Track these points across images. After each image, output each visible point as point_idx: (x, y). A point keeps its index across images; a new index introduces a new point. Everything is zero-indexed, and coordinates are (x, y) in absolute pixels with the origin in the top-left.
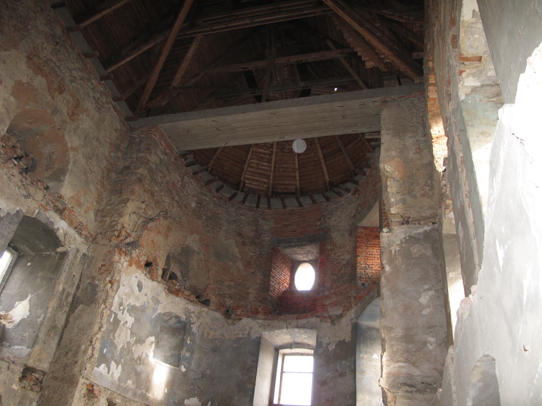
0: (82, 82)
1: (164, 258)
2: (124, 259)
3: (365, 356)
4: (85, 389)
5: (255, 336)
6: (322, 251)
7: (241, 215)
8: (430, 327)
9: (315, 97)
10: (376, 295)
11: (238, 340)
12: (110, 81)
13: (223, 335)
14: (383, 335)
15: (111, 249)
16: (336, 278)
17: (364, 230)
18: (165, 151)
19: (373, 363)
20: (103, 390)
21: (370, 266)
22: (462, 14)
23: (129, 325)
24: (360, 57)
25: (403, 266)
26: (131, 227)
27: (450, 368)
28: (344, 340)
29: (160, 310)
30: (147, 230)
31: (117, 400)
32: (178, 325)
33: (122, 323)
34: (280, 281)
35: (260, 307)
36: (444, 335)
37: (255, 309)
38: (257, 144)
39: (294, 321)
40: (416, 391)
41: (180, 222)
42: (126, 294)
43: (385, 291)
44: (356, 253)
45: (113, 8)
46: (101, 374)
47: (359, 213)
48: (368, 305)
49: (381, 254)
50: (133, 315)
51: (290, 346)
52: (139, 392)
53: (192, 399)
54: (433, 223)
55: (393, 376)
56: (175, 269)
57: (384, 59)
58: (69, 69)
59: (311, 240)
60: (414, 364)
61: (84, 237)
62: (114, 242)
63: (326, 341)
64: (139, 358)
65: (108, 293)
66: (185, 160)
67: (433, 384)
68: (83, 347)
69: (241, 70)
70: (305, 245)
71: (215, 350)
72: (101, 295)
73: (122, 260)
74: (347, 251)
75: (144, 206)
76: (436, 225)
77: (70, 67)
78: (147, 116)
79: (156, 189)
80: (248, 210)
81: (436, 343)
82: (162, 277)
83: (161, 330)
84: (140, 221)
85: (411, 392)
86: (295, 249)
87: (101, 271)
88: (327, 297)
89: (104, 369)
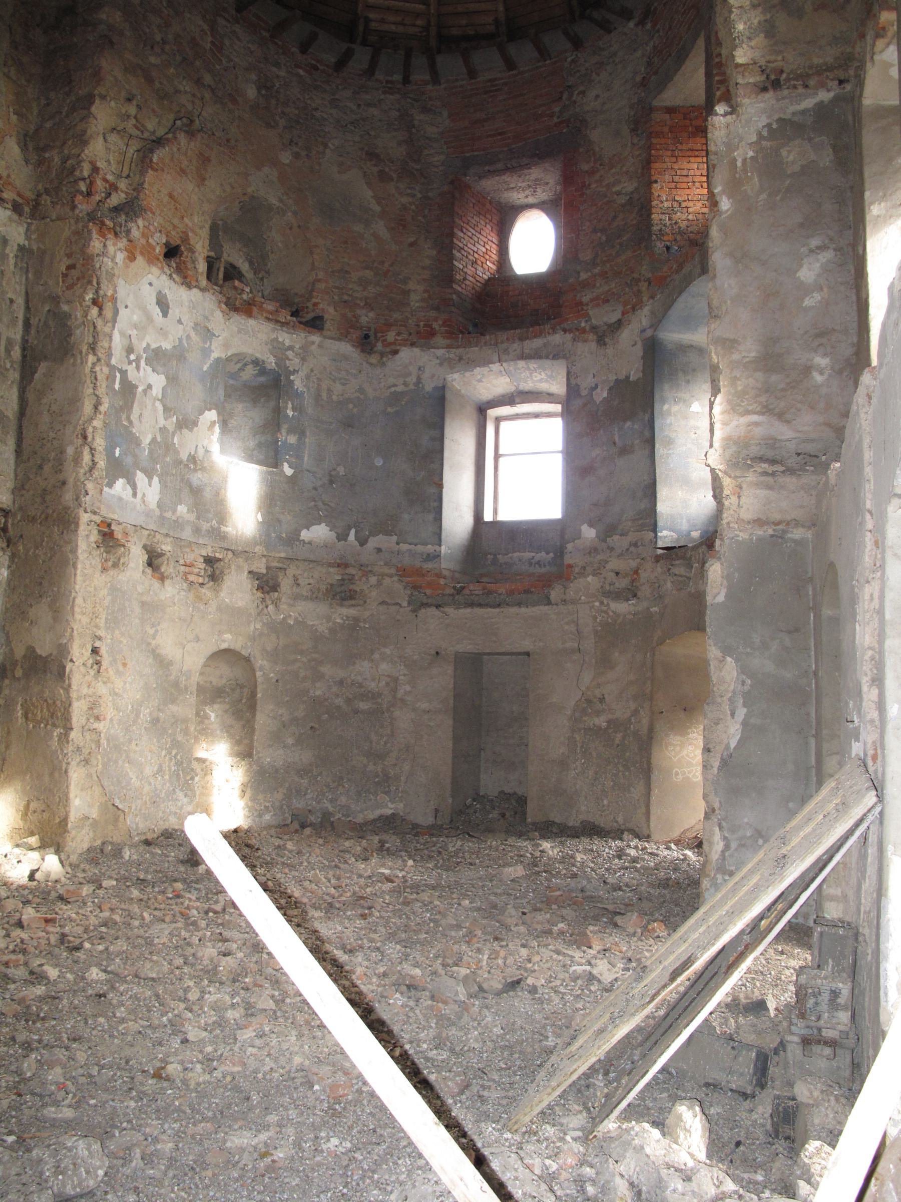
1: (205, 233)
2: (114, 245)
3: (675, 408)
4: (96, 532)
5: (433, 385)
6: (568, 178)
7: (369, 105)
8: (821, 335)
10: (698, 270)
11: (396, 397)
13: (361, 390)
14: (715, 359)
15: (80, 225)
16: (604, 238)
17: (667, 116)
19: (692, 423)
20: (131, 530)
21: (684, 205)
23: (157, 391)
25: (764, 196)
26: (114, 167)
27: (862, 415)
28: (628, 377)
29: (217, 353)
30: (153, 169)
31: (164, 547)
32: (262, 379)
33: (140, 389)
34: (476, 257)
35: (436, 319)
36: (850, 351)
37: (425, 325)
39: (515, 346)
40: (783, 472)
41: (228, 140)
42: (135, 326)
43: (719, 259)
44: (650, 175)
46: (120, 499)
47: (655, 73)
48: (680, 293)
49: (710, 170)
50: (160, 369)
51: (509, 400)
52: (205, 526)
53: (314, 528)
54: (841, 82)
55: (735, 443)
56: (234, 255)
59: (540, 153)
60: (780, 416)
61: (10, 206)
62: (83, 207)
63: (586, 383)
64: (193, 459)
65: (95, 327)
67: (820, 455)
68: (70, 450)
70: (528, 166)
71: (349, 424)
72: (82, 336)
73: (111, 249)
74: (627, 172)
75: (133, 110)
76: (848, 87)
79: (153, 60)
80: (384, 93)
81: (832, 368)
82: (209, 278)
83: (228, 396)
84: (131, 150)
85: (773, 474)
86: (506, 177)
87: (69, 281)
88: (585, 285)
89: (124, 489)
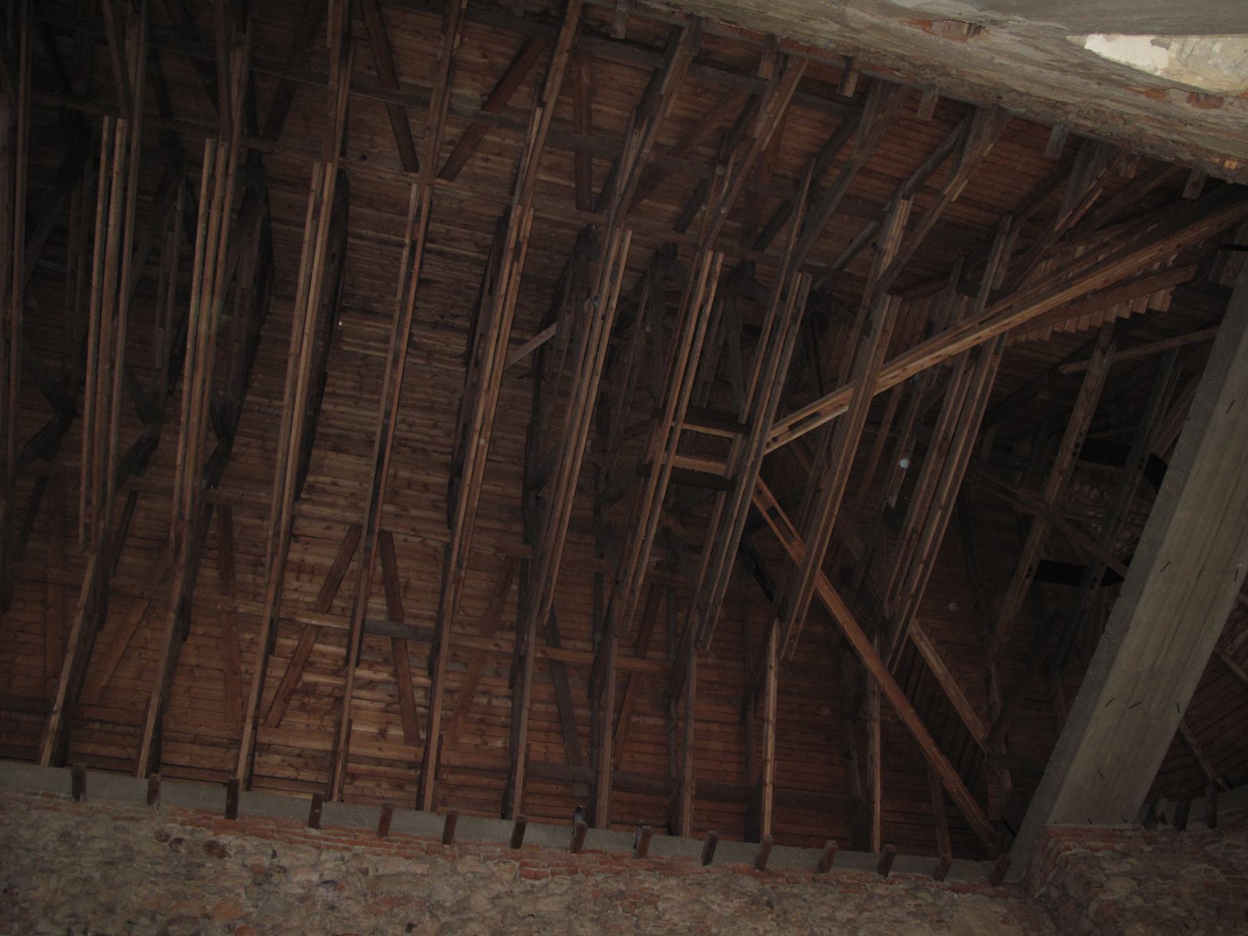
0: (867, 914)
9: (1175, 454)
12: (899, 860)
18: (1115, 851)
22: (1148, 70)
24: (1133, 314)
38: (1220, 640)
45: (769, 756)
57: (1163, 265)
58: (829, 919)
66: (1165, 823)
69: (1028, 582)
77: (824, 915)
78: (1015, 835)
